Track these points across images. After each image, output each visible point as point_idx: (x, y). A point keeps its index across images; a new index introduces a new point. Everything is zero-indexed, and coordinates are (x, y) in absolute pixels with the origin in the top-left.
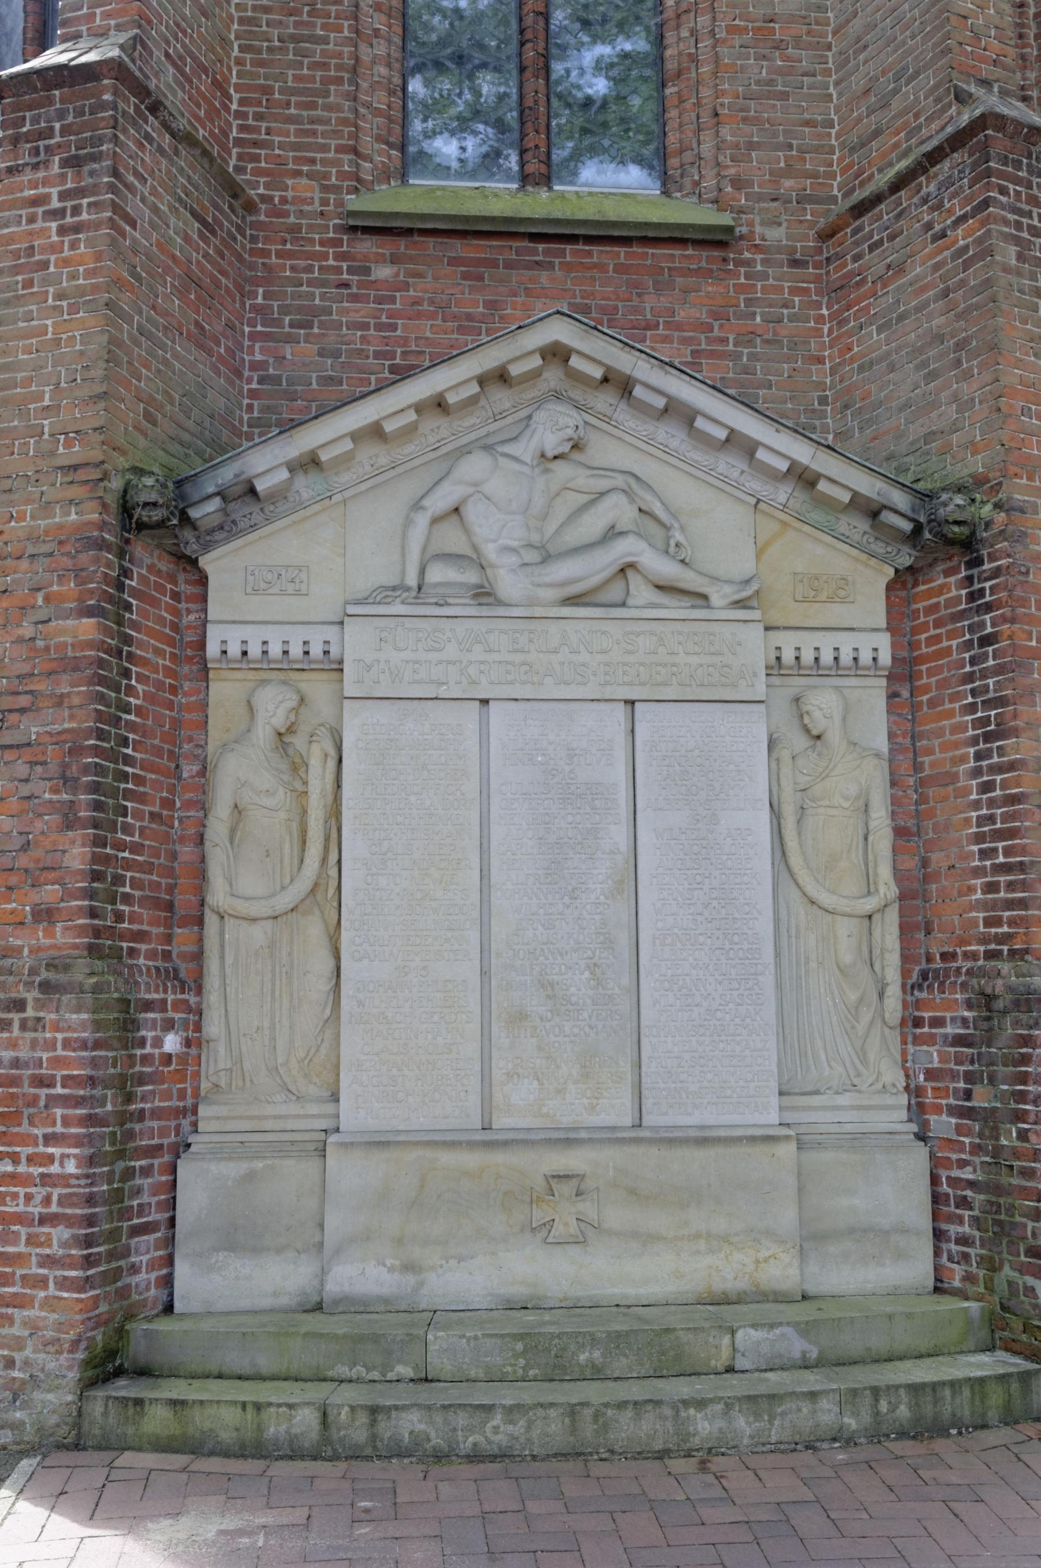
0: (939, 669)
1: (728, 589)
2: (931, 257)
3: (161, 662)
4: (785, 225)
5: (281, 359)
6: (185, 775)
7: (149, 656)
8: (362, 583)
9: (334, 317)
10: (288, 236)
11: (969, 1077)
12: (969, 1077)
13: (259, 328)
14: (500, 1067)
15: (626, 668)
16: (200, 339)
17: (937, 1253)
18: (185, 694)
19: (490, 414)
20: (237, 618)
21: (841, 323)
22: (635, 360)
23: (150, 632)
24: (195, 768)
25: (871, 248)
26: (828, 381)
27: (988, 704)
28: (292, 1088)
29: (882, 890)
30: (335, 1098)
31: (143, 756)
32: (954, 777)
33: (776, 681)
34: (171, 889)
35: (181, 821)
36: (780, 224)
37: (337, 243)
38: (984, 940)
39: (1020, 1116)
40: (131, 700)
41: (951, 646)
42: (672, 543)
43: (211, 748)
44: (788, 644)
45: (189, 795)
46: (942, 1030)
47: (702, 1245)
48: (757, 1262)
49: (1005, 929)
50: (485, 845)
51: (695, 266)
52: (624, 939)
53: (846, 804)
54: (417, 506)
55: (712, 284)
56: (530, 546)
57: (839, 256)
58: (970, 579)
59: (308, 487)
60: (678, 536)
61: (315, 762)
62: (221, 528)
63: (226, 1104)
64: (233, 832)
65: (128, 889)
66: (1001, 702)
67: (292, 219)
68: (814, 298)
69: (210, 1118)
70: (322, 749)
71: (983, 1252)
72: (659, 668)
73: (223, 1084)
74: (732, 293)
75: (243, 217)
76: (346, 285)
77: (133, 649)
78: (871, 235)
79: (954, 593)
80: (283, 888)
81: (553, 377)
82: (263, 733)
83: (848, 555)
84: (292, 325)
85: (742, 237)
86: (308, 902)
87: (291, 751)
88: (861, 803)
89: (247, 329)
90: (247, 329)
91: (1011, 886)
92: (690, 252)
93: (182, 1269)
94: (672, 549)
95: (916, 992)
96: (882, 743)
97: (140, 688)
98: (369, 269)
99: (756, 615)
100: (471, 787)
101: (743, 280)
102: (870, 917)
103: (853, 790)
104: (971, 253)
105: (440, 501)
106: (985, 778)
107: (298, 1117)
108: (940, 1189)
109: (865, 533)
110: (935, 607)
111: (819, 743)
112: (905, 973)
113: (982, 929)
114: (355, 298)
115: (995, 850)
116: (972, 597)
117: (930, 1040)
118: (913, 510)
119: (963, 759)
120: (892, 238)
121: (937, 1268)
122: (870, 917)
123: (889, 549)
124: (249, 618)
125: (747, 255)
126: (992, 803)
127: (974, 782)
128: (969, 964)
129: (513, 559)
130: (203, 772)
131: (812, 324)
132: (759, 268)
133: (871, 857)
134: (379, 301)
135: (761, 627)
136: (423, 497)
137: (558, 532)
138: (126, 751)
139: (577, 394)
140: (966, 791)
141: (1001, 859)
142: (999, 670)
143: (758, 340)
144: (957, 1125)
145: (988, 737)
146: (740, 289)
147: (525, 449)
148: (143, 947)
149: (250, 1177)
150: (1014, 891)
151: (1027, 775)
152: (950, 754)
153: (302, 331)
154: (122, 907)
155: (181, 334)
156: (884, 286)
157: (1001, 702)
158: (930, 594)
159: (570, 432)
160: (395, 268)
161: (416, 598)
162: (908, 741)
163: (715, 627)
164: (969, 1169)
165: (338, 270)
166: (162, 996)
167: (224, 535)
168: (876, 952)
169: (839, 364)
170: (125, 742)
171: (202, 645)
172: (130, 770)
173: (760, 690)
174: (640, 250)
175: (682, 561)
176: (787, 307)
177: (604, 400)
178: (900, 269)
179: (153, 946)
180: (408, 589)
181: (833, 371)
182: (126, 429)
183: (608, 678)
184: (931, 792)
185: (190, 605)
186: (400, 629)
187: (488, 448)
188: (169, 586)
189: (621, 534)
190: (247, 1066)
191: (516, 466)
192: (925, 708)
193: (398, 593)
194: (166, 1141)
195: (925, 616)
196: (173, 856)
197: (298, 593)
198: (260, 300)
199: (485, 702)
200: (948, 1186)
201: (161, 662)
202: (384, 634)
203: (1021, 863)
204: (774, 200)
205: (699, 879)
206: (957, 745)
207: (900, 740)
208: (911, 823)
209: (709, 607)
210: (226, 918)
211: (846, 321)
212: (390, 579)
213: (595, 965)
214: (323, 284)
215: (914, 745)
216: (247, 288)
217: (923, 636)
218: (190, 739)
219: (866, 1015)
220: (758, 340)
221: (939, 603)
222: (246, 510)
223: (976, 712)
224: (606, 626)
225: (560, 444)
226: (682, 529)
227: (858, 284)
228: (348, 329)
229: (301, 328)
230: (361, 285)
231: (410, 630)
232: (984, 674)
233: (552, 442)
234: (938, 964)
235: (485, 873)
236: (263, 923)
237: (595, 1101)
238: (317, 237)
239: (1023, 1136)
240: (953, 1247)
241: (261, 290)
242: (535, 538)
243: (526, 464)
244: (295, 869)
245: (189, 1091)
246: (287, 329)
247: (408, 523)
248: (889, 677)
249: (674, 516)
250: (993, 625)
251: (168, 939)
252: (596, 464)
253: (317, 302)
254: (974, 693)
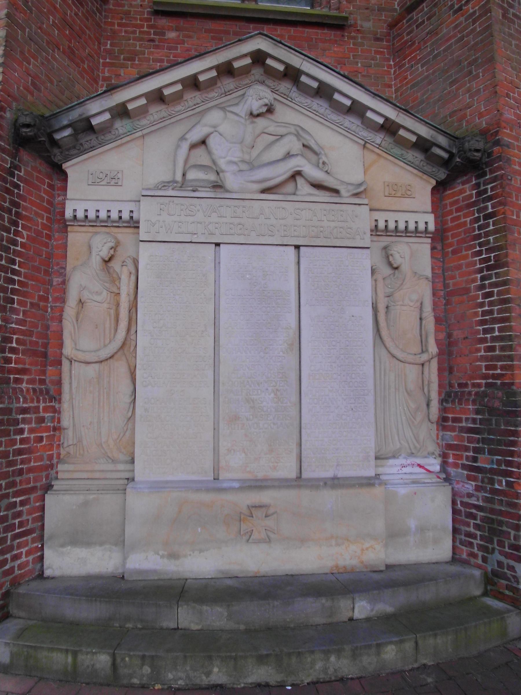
0: (459, 234)
1: (350, 188)
2: (452, 22)
3: (40, 221)
4: (372, 21)
5: (118, 76)
6: (55, 283)
7: (32, 216)
8: (152, 180)
9: (146, 56)
10: (124, 16)
11: (476, 450)
12: (476, 450)
13: (108, 60)
14: (224, 445)
15: (295, 228)
16: (71, 54)
17: (454, 541)
18: (56, 240)
19: (223, 91)
20: (83, 198)
21: (400, 68)
22: (301, 61)
23: (32, 203)
24: (60, 280)
25: (417, 27)
26: (394, 96)
27: (489, 250)
28: (110, 455)
29: (430, 350)
30: (133, 461)
31: (26, 271)
32: (467, 290)
33: (375, 238)
34: (45, 346)
35: (52, 309)
36: (370, 21)
37: (149, 20)
38: (485, 377)
39: (510, 474)
40: (18, 238)
41: (466, 221)
42: (321, 161)
43: (68, 268)
44: (381, 218)
45: (56, 295)
46: (460, 425)
47: (333, 542)
48: (362, 550)
49: (499, 371)
50: (217, 324)
51: (328, 38)
52: (293, 376)
53: (412, 304)
54: (183, 138)
55: (337, 47)
56: (243, 161)
57: (399, 35)
58: (478, 185)
59: (122, 126)
60: (324, 159)
61: (124, 277)
62: (74, 147)
63: (73, 463)
64: (78, 314)
65: (14, 345)
66: (499, 248)
67: (126, 8)
68: (387, 56)
69: (64, 471)
70: (128, 270)
71: (482, 543)
72: (313, 228)
73: (72, 452)
74: (346, 52)
75: (101, 6)
76: (152, 40)
77: (20, 210)
78: (417, 20)
79: (468, 193)
80: (105, 346)
81: (257, 72)
82: (96, 261)
83: (412, 173)
84: (124, 59)
85: (351, 26)
86: (120, 353)
87: (111, 271)
88: (418, 304)
89: (101, 61)
90: (101, 61)
91: (502, 348)
92: (326, 31)
93: (48, 553)
94: (321, 165)
95: (444, 404)
96: (428, 273)
97: (25, 233)
98: (165, 33)
99: (365, 201)
100: (211, 289)
101: (352, 46)
102: (423, 365)
103: (415, 297)
104: (477, 14)
105: (195, 136)
106: (487, 290)
107: (112, 471)
108: (456, 507)
109: (422, 160)
110: (457, 201)
111: (396, 271)
112: (440, 394)
113: (484, 371)
114: (157, 47)
115: (493, 329)
116: (479, 194)
117: (453, 429)
118: (450, 146)
119: (474, 280)
120: (429, 19)
121: (454, 548)
122: (423, 365)
123: (434, 170)
124: (89, 198)
125: (353, 34)
126: (491, 304)
127: (480, 293)
128: (476, 390)
129: (235, 168)
130: (64, 283)
131: (386, 68)
132: (359, 40)
133: (423, 333)
134: (169, 48)
135: (367, 208)
136: (186, 134)
137: (259, 155)
138: (13, 267)
139: (269, 82)
140: (477, 297)
141: (497, 333)
142: (495, 231)
143: (359, 75)
144: (467, 475)
145: (489, 268)
146: (351, 50)
147: (242, 109)
148: (26, 377)
149: (86, 504)
150: (505, 351)
151: (513, 288)
152: (465, 278)
153: (129, 63)
154: (10, 355)
155: (59, 49)
156: (425, 43)
157: (499, 248)
158: (453, 195)
159: (266, 101)
160: (178, 33)
161: (181, 187)
162: (441, 272)
163: (344, 207)
164: (474, 498)
165: (149, 33)
166: (36, 404)
167: (75, 152)
168: (426, 383)
169: (400, 87)
170: (13, 262)
171: (63, 213)
172: (16, 278)
173: (367, 241)
174: (301, 29)
175: (326, 172)
176: (373, 60)
177: (285, 86)
178: (433, 33)
179: (33, 376)
180: (177, 182)
181: (396, 91)
182: (18, 88)
183: (286, 233)
184: (454, 299)
185: (59, 192)
186: (171, 203)
187: (223, 109)
188: (47, 180)
189: (293, 155)
190: (85, 442)
191: (236, 118)
192: (450, 255)
193: (171, 184)
194: (38, 484)
195: (451, 207)
196: (47, 327)
197: (116, 185)
198: (108, 46)
199: (218, 245)
200: (461, 505)
201: (40, 221)
202: (162, 206)
203: (510, 335)
204: (367, 9)
205: (334, 343)
206: (470, 274)
207: (437, 271)
208: (442, 315)
209: (340, 197)
210: (73, 362)
211: (404, 65)
212: (168, 177)
213: (277, 390)
214: (141, 39)
215: (443, 274)
216: (102, 41)
217: (449, 218)
218: (58, 264)
219: (419, 417)
220: (359, 75)
221: (459, 199)
222: (88, 138)
223: (482, 255)
224: (283, 204)
225: (261, 107)
226: (326, 155)
227: (411, 46)
228: (153, 62)
229: (129, 61)
230: (160, 41)
231: (177, 204)
232: (487, 234)
233: (256, 106)
234: (456, 388)
235: (216, 339)
236: (93, 365)
237: (276, 464)
238: (138, 17)
239: (509, 484)
240: (463, 537)
241: (109, 42)
242: (247, 157)
243: (242, 117)
244: (112, 335)
245: (55, 456)
246: (122, 61)
247: (178, 146)
248: (433, 239)
249: (322, 149)
250: (492, 208)
251: (44, 373)
252: (280, 121)
253: (138, 48)
254: (480, 245)
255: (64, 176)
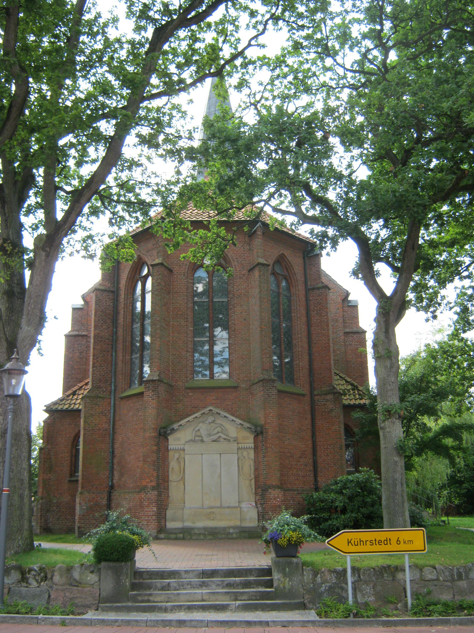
8: (187, 440)
44: (240, 445)
54: (194, 430)
82: (175, 459)
96: (253, 458)
105: (197, 429)
147: (207, 422)
233: (210, 421)
255: (168, 439)
